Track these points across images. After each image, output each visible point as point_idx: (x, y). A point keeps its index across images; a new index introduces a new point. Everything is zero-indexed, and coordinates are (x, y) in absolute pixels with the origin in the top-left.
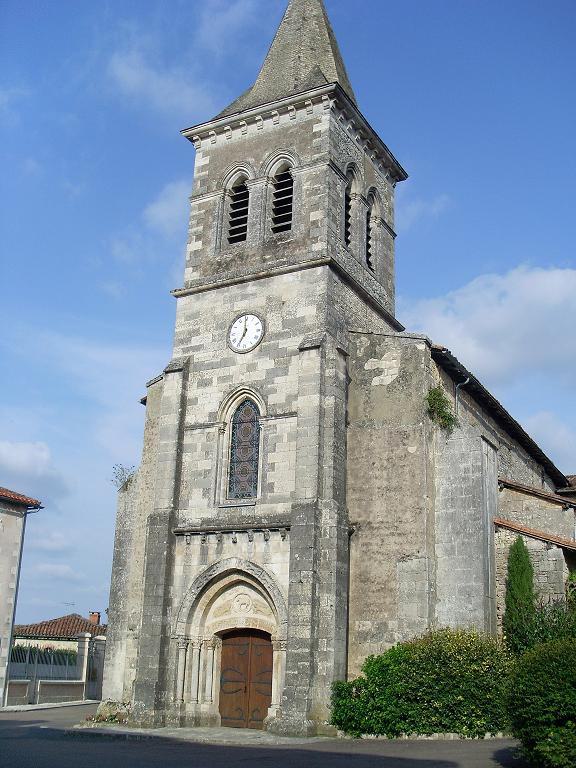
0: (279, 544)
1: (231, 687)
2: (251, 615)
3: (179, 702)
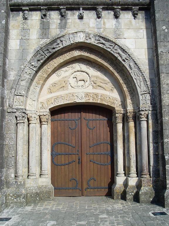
0: (130, 22)
1: (63, 159)
2: (90, 90)
3: (136, 74)
